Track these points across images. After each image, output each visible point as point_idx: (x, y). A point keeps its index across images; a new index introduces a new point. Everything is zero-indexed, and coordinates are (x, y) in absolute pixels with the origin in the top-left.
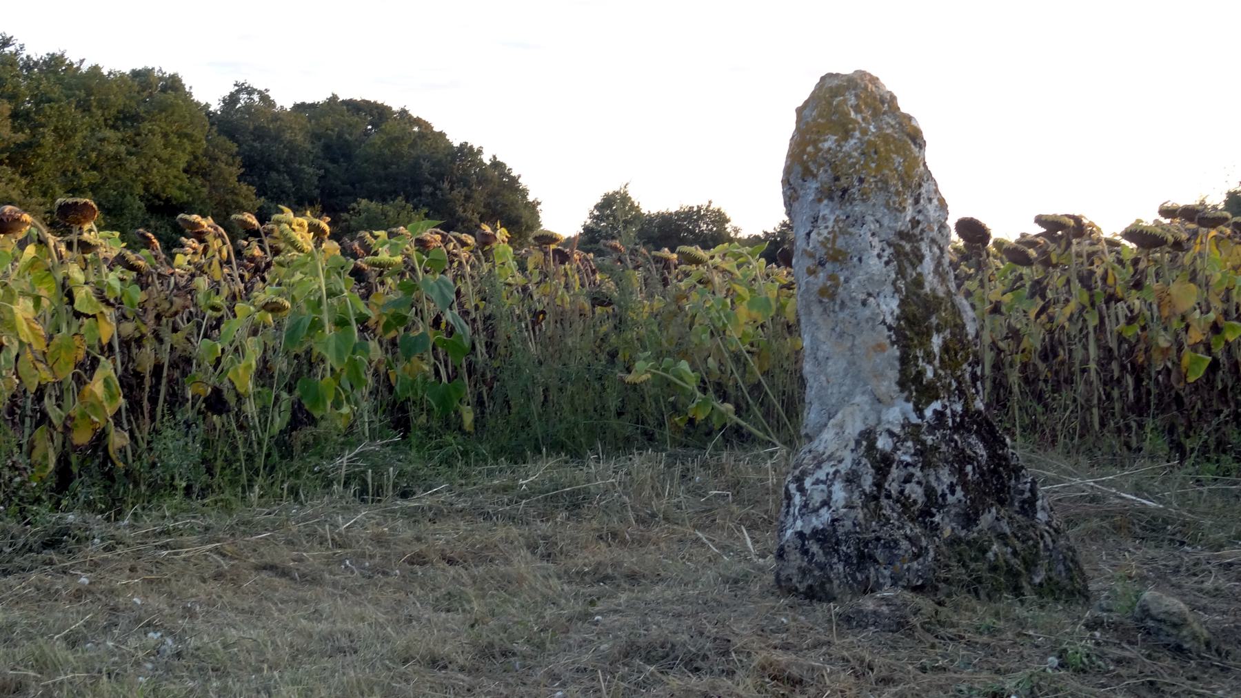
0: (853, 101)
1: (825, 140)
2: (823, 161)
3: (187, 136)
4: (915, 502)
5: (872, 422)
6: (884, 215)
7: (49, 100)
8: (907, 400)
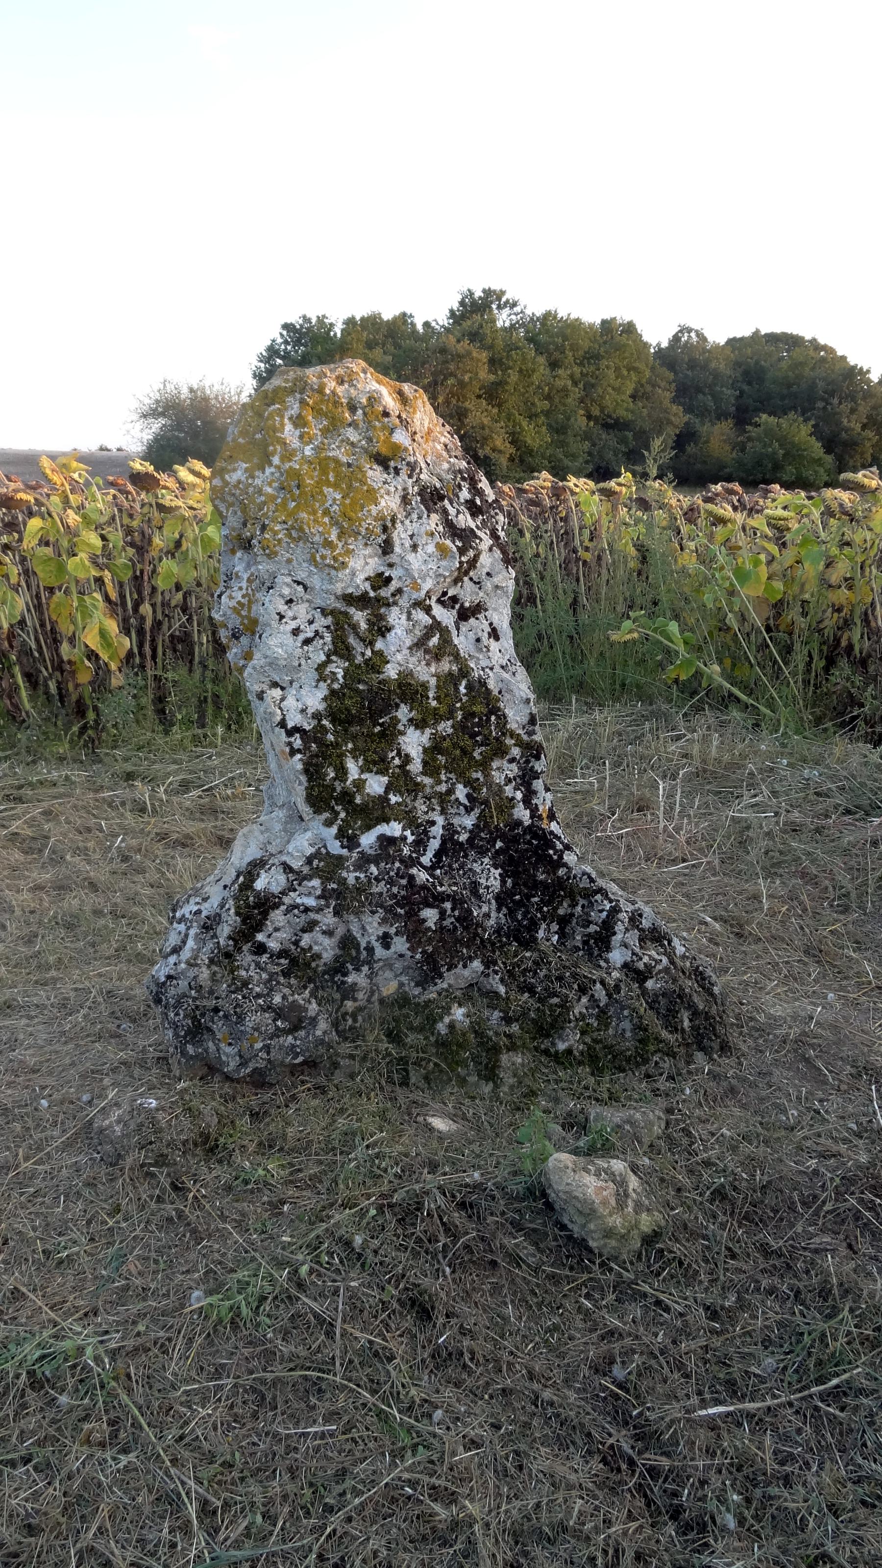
0: (295, 409)
1: (235, 470)
2: (230, 499)
3: (635, 369)
4: (318, 956)
5: (272, 849)
6: (311, 573)
7: (517, 348)
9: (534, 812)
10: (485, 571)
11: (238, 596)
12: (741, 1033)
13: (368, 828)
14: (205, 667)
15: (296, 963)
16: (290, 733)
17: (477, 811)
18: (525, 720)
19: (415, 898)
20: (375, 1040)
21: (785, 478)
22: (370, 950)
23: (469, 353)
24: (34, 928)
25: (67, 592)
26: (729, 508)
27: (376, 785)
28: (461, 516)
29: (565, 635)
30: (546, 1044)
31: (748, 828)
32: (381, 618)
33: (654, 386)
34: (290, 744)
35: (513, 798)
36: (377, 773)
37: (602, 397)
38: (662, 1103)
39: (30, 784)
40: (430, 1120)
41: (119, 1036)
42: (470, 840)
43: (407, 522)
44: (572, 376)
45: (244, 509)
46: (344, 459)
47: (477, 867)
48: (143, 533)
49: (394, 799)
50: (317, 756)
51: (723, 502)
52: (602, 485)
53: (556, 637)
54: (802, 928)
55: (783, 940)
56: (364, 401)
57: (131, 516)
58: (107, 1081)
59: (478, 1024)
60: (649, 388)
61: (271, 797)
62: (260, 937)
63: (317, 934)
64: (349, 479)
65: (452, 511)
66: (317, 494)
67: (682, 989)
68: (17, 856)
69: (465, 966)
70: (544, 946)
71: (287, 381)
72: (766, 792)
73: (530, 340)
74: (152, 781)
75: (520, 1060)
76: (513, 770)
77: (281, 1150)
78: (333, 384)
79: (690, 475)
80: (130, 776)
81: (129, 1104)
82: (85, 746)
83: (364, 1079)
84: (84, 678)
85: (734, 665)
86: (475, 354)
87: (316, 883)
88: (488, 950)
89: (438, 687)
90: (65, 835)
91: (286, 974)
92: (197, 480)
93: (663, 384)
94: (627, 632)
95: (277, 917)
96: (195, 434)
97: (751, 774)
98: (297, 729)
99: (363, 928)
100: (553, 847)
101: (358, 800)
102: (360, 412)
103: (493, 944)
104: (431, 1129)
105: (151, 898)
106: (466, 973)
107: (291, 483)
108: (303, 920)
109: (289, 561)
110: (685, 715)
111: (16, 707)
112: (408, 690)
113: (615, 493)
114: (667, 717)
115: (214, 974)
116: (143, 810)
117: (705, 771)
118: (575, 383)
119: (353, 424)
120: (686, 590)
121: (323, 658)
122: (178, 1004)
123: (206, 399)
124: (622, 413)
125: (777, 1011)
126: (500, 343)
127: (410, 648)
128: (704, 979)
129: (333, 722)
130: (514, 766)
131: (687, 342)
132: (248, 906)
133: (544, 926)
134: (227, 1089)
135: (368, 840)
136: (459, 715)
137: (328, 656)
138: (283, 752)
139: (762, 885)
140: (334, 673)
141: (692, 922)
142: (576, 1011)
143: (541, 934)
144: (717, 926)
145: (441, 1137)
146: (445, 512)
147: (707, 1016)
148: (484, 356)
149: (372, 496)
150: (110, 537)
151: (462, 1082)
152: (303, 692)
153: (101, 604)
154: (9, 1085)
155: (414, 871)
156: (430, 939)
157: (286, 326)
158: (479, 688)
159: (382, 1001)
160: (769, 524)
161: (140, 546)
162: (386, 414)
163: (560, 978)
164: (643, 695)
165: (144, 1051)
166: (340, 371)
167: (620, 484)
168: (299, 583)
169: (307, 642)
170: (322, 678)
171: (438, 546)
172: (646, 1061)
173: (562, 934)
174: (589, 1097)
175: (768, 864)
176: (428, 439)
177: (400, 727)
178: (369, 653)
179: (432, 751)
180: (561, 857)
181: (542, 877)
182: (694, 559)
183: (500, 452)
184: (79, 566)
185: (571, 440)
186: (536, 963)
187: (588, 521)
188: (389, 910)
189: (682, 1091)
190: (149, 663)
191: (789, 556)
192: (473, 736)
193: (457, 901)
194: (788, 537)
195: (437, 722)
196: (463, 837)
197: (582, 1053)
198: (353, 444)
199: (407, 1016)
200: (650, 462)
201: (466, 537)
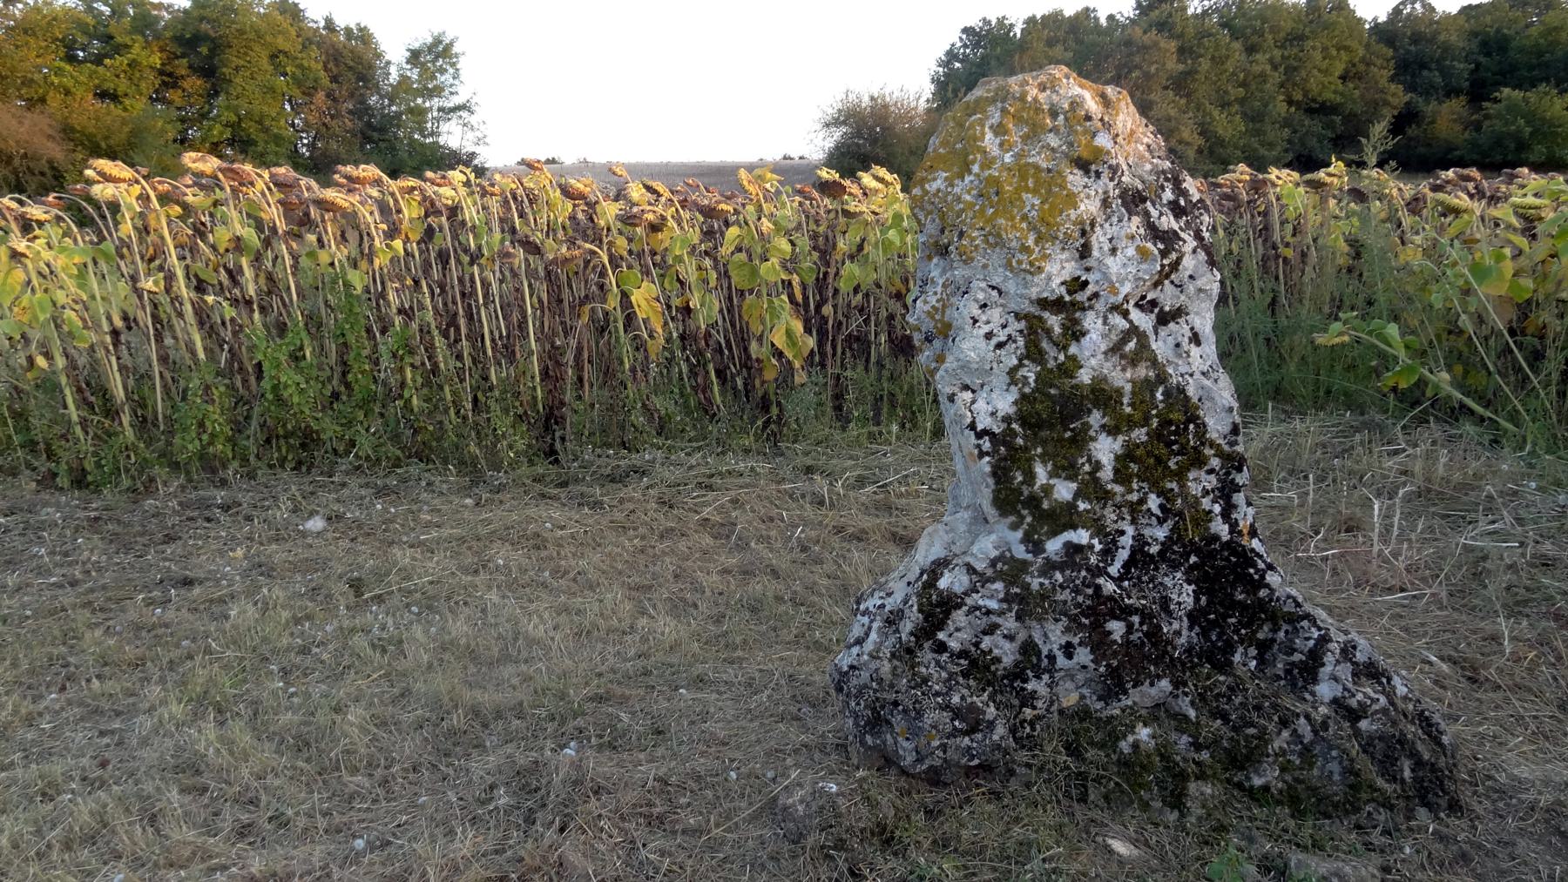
1: (935, 179)
2: (930, 207)
3: (1347, 48)
4: (998, 660)
8: (1014, 527)
9: (1234, 527)
10: (1188, 273)
11: (933, 300)
12: (1475, 793)
13: (1054, 533)
14: (883, 366)
15: (977, 665)
16: (979, 435)
17: (1170, 523)
18: (1227, 429)
19: (1100, 609)
20: (1053, 752)
21: (1532, 158)
22: (1052, 658)
23: (1156, 44)
24: (722, 609)
25: (759, 295)
26: (1466, 197)
27: (1064, 491)
28: (1164, 218)
29: (1261, 338)
30: (1239, 777)
31: (1485, 558)
32: (1076, 322)
33: (1368, 65)
34: (978, 446)
35: (1210, 512)
36: (1066, 479)
37: (1306, 80)
38: (1376, 859)
39: (720, 474)
40: (1110, 841)
41: (799, 719)
42: (1161, 553)
43: (1107, 225)
44: (1271, 61)
45: (943, 217)
46: (1044, 165)
47: (1168, 581)
48: (827, 238)
49: (1082, 506)
50: (1005, 459)
51: (1458, 191)
52: (1309, 176)
53: (1250, 338)
54: (1555, 679)
55: (1530, 690)
56: (1066, 106)
57: (817, 222)
58: (789, 761)
59: (1165, 747)
60: (1362, 67)
61: (955, 498)
62: (941, 636)
63: (997, 637)
64: (1048, 184)
65: (1154, 213)
66: (1016, 200)
67: (1403, 734)
68: (708, 540)
69: (1152, 684)
70: (1240, 671)
71: (988, 91)
72: (1508, 518)
73: (1224, 25)
74: (831, 476)
75: (1209, 791)
76: (1211, 482)
77: (956, 850)
78: (1036, 91)
79: (1415, 158)
80: (809, 470)
81: (814, 786)
82: (768, 439)
83: (1040, 790)
84: (770, 375)
85: (1466, 373)
86: (1162, 45)
87: (999, 586)
88: (1179, 670)
89: (1133, 393)
90: (750, 523)
91: (965, 675)
92: (880, 186)
93: (1379, 62)
94: (1335, 335)
95: (959, 617)
96: (874, 141)
97: (1490, 497)
98: (985, 432)
99: (1046, 635)
100: (1254, 565)
101: (1045, 505)
102: (1061, 117)
103: (1183, 664)
104: (1111, 851)
105: (828, 589)
106: (1153, 691)
107: (990, 191)
108: (984, 622)
109: (985, 266)
110: (1404, 428)
111: (709, 400)
112: (1102, 396)
113: (1325, 184)
114: (1381, 428)
115: (895, 668)
116: (821, 503)
117: (1429, 491)
118: (1275, 68)
119: (1054, 130)
120: (1410, 289)
121: (1015, 362)
122: (860, 694)
123: (886, 106)
124: (1328, 95)
125: (1523, 772)
126: (1191, 31)
127: (1105, 353)
128: (1430, 725)
129: (1022, 426)
130: (1213, 478)
131: (1409, 15)
132: (931, 604)
133: (1241, 649)
134: (903, 783)
135: (1054, 546)
136: (1155, 423)
137: (1020, 360)
138: (971, 454)
139: (1504, 625)
140: (1026, 378)
141: (1412, 660)
142: (1276, 745)
143: (1237, 658)
144: (1445, 667)
145: (1121, 862)
146: (1147, 214)
147: (1433, 768)
148: (1173, 45)
149: (1072, 200)
150: (798, 242)
151: (1145, 806)
152: (994, 396)
153: (788, 306)
154: (702, 754)
155: (1101, 581)
156: (1115, 653)
157: (965, 30)
158: (1177, 395)
159: (1061, 712)
160: (1516, 213)
161: (824, 249)
162: (1088, 118)
163: (1258, 708)
164: (1352, 403)
165: (823, 736)
166: (1043, 78)
167: (1330, 175)
168: (993, 288)
169: (1000, 346)
170: (1013, 382)
171: (1138, 249)
172: (1357, 810)
173: (1261, 659)
174: (1289, 842)
175: (1511, 602)
176: (1131, 139)
177: (1092, 433)
178: (1062, 357)
179: (1123, 460)
180: (1263, 577)
181: (1241, 597)
182: (1419, 255)
183: (1188, 144)
184: (771, 270)
185: (1268, 128)
186: (1230, 688)
187: (1291, 214)
188: (1073, 619)
189: (1401, 849)
190: (829, 362)
191: (1542, 249)
192: (1169, 444)
193: (1146, 616)
194: (1540, 228)
195: (1131, 429)
196: (1154, 549)
197: (1281, 792)
198: (1053, 150)
199: (1088, 730)
200: (1368, 150)
201: (1168, 240)
